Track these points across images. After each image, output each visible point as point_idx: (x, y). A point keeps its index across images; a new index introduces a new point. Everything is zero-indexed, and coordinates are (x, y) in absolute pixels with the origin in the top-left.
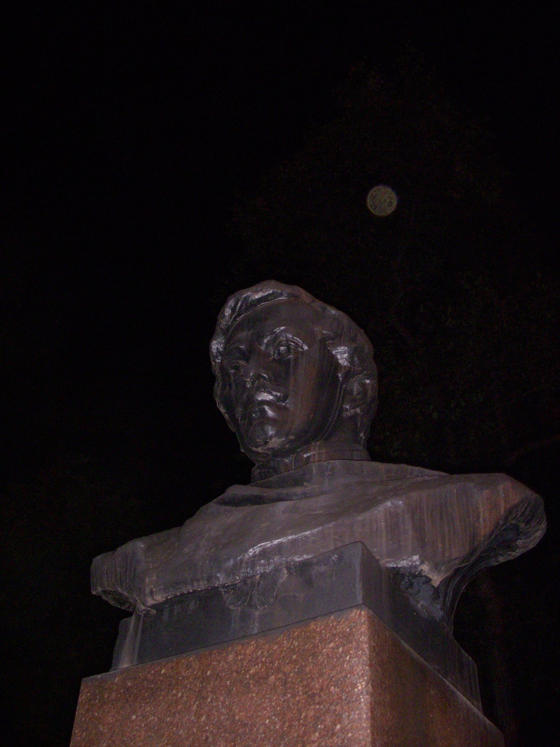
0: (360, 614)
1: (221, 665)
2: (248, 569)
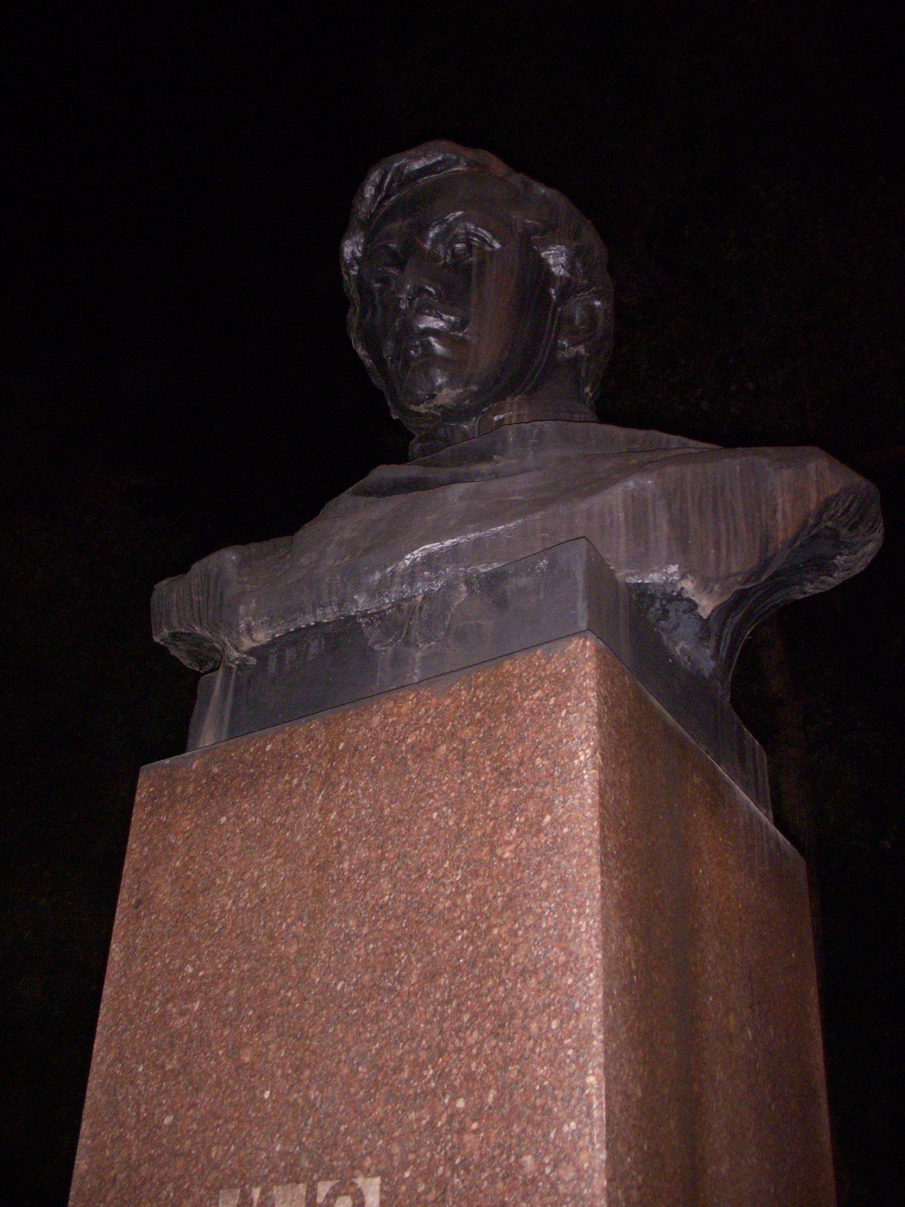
0: (584, 646)
1: (360, 733)
2: (404, 586)
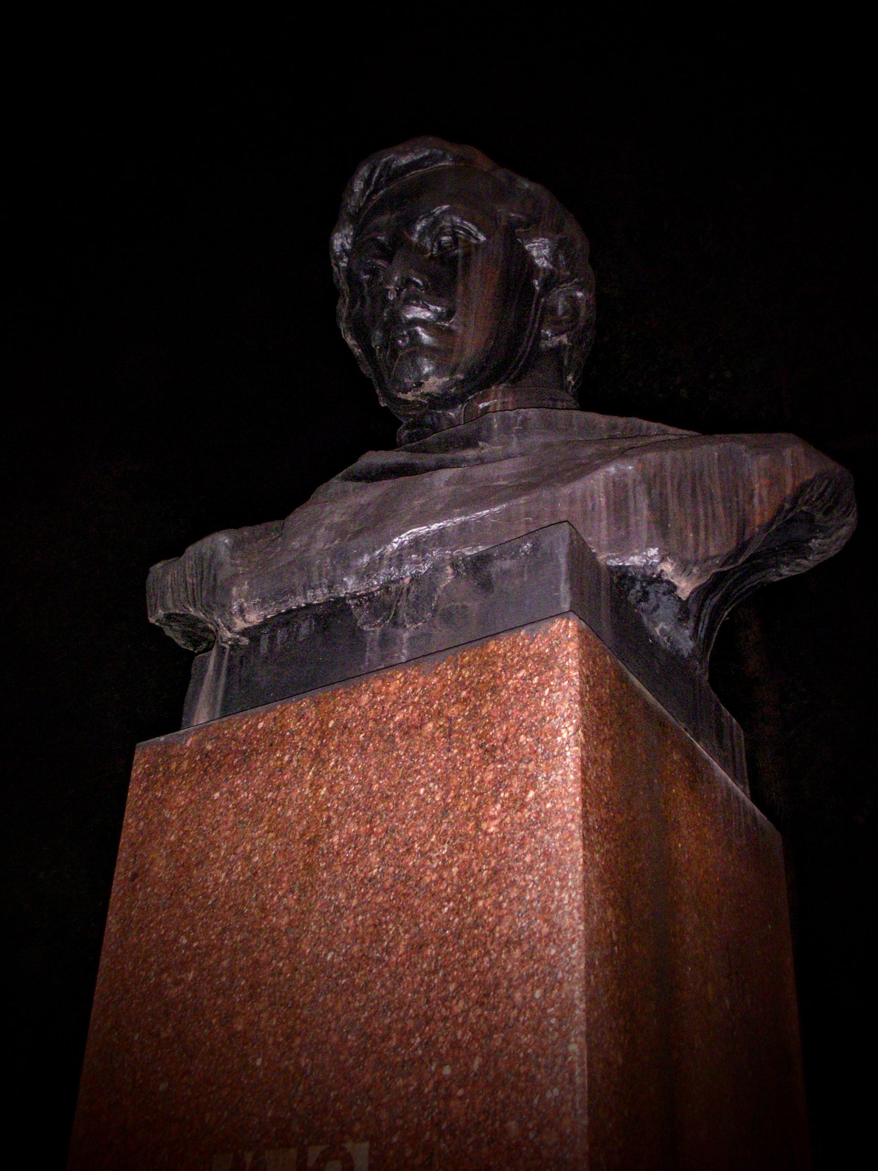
0: (566, 626)
1: (350, 711)
